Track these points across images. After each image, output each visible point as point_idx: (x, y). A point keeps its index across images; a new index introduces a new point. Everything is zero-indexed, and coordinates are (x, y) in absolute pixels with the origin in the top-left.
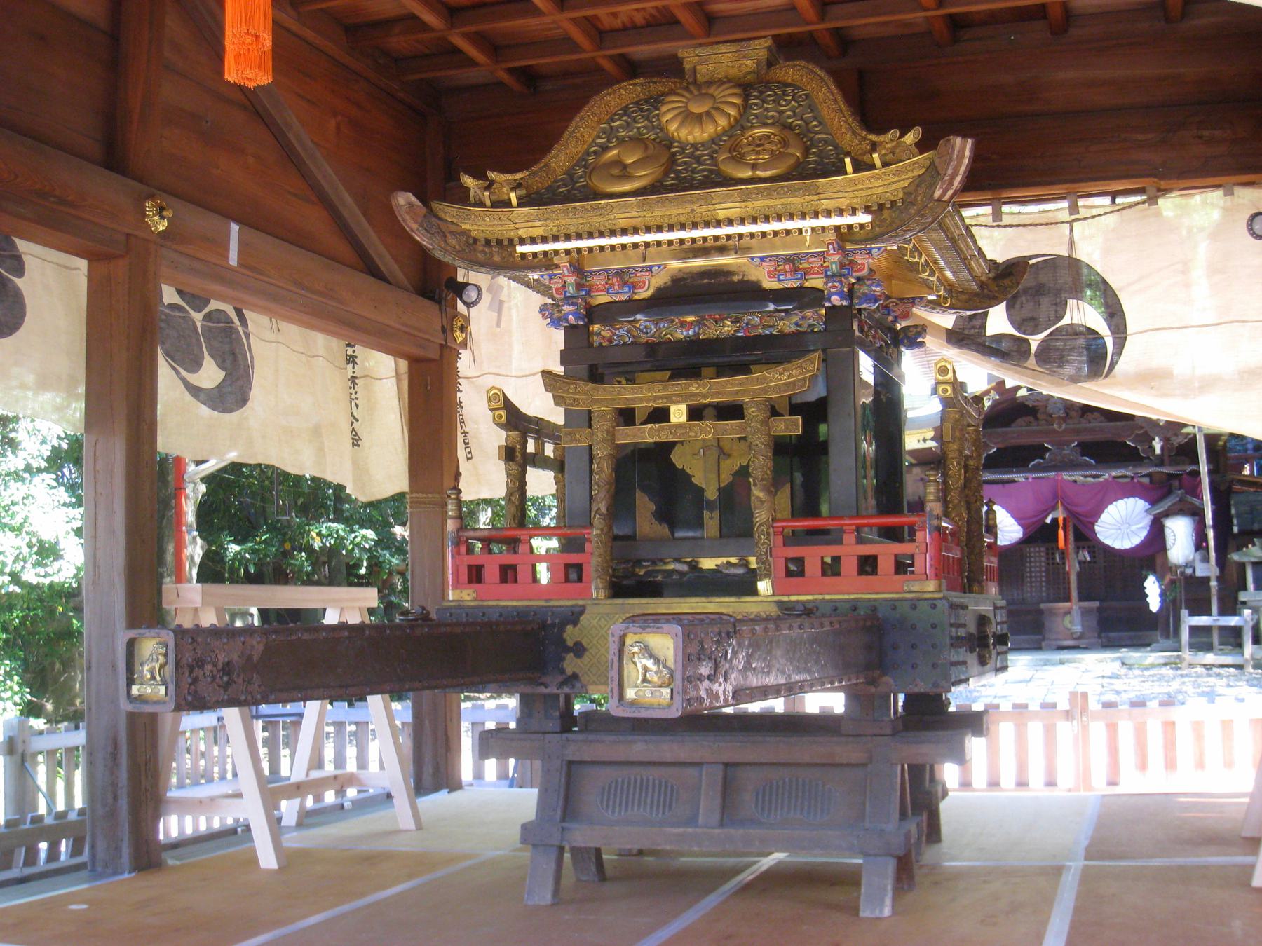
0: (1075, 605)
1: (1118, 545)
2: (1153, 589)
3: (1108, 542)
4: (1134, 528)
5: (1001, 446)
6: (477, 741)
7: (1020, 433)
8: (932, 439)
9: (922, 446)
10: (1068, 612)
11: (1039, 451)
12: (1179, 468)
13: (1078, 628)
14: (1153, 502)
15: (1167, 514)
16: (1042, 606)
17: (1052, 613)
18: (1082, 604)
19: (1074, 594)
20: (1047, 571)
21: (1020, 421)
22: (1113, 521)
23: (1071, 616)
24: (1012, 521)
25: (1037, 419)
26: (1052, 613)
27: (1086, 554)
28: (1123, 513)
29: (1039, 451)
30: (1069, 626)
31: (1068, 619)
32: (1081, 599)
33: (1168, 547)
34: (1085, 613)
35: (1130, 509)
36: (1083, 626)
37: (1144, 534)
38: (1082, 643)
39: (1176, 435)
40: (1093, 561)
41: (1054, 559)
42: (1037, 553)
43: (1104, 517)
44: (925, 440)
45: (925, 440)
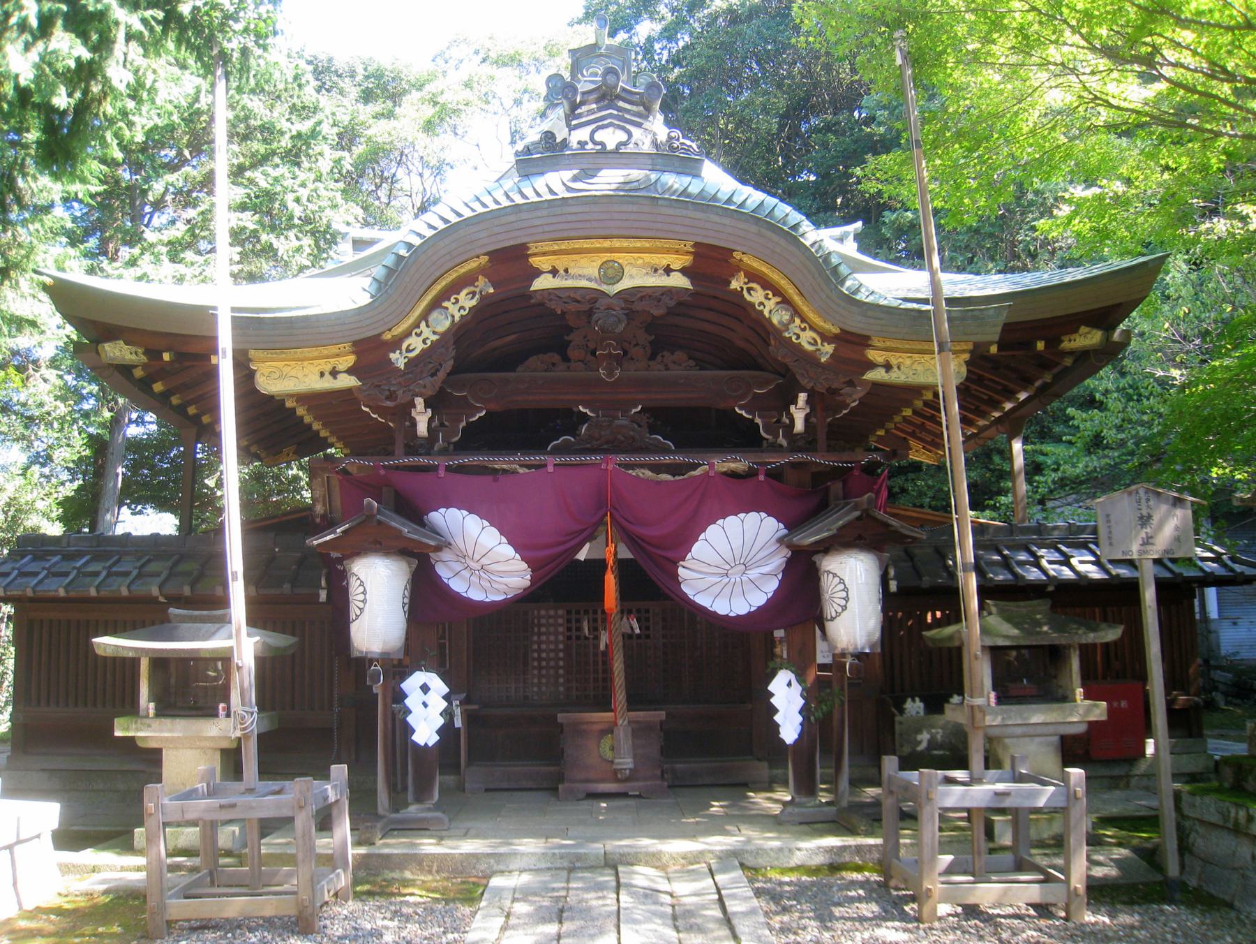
0: (620, 717)
1: (721, 607)
2: (787, 699)
3: (703, 600)
4: (753, 573)
5: (494, 407)
6: (164, 655)
7: (534, 383)
8: (350, 371)
9: (328, 384)
10: (610, 730)
11: (569, 421)
12: (846, 456)
13: (626, 762)
14: (793, 524)
15: (827, 547)
16: (561, 717)
17: (579, 731)
18: (640, 715)
19: (620, 696)
20: (567, 649)
21: (533, 361)
22: (715, 559)
23: (615, 738)
24: (509, 551)
25: (566, 359)
26: (579, 731)
27: (635, 624)
28: (737, 544)
29: (569, 421)
30: (609, 755)
31: (606, 742)
32: (635, 701)
33: (830, 609)
34: (639, 731)
35: (749, 536)
36: (635, 757)
37: (772, 585)
38: (633, 787)
39: (851, 383)
40: (645, 635)
41: (579, 629)
42: (552, 618)
43: (699, 549)
44: (334, 373)
45: (334, 373)
